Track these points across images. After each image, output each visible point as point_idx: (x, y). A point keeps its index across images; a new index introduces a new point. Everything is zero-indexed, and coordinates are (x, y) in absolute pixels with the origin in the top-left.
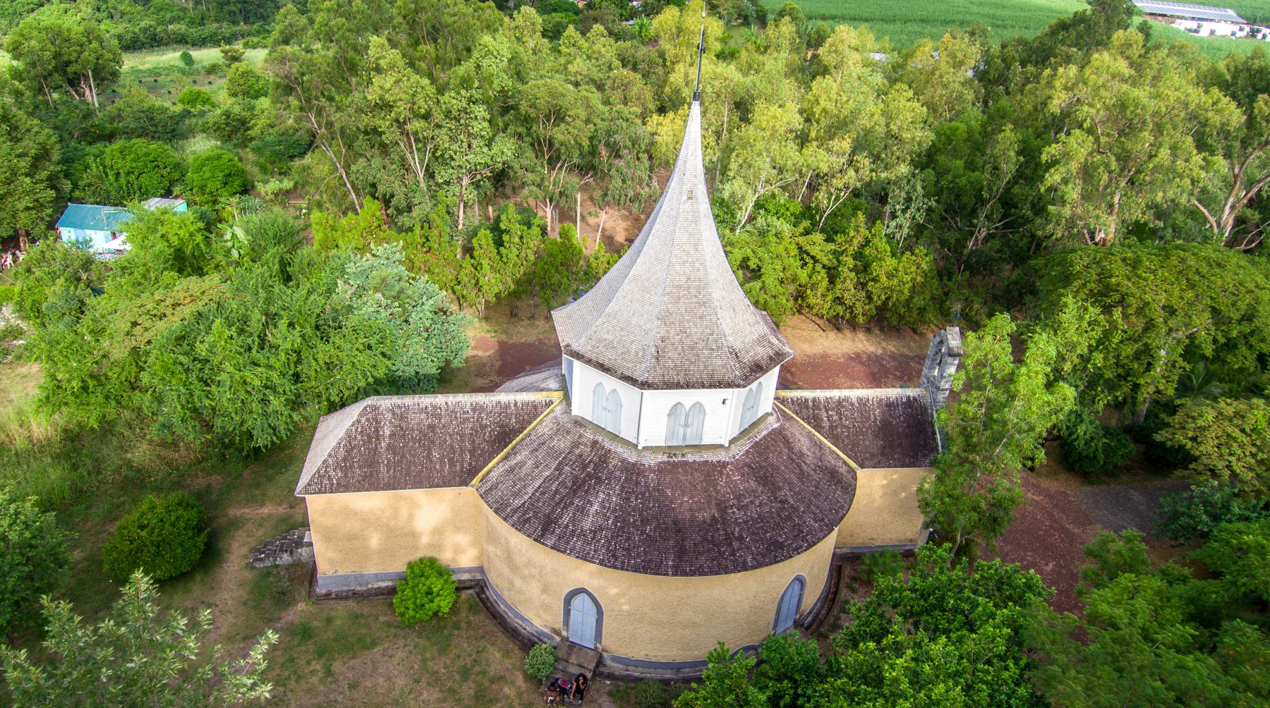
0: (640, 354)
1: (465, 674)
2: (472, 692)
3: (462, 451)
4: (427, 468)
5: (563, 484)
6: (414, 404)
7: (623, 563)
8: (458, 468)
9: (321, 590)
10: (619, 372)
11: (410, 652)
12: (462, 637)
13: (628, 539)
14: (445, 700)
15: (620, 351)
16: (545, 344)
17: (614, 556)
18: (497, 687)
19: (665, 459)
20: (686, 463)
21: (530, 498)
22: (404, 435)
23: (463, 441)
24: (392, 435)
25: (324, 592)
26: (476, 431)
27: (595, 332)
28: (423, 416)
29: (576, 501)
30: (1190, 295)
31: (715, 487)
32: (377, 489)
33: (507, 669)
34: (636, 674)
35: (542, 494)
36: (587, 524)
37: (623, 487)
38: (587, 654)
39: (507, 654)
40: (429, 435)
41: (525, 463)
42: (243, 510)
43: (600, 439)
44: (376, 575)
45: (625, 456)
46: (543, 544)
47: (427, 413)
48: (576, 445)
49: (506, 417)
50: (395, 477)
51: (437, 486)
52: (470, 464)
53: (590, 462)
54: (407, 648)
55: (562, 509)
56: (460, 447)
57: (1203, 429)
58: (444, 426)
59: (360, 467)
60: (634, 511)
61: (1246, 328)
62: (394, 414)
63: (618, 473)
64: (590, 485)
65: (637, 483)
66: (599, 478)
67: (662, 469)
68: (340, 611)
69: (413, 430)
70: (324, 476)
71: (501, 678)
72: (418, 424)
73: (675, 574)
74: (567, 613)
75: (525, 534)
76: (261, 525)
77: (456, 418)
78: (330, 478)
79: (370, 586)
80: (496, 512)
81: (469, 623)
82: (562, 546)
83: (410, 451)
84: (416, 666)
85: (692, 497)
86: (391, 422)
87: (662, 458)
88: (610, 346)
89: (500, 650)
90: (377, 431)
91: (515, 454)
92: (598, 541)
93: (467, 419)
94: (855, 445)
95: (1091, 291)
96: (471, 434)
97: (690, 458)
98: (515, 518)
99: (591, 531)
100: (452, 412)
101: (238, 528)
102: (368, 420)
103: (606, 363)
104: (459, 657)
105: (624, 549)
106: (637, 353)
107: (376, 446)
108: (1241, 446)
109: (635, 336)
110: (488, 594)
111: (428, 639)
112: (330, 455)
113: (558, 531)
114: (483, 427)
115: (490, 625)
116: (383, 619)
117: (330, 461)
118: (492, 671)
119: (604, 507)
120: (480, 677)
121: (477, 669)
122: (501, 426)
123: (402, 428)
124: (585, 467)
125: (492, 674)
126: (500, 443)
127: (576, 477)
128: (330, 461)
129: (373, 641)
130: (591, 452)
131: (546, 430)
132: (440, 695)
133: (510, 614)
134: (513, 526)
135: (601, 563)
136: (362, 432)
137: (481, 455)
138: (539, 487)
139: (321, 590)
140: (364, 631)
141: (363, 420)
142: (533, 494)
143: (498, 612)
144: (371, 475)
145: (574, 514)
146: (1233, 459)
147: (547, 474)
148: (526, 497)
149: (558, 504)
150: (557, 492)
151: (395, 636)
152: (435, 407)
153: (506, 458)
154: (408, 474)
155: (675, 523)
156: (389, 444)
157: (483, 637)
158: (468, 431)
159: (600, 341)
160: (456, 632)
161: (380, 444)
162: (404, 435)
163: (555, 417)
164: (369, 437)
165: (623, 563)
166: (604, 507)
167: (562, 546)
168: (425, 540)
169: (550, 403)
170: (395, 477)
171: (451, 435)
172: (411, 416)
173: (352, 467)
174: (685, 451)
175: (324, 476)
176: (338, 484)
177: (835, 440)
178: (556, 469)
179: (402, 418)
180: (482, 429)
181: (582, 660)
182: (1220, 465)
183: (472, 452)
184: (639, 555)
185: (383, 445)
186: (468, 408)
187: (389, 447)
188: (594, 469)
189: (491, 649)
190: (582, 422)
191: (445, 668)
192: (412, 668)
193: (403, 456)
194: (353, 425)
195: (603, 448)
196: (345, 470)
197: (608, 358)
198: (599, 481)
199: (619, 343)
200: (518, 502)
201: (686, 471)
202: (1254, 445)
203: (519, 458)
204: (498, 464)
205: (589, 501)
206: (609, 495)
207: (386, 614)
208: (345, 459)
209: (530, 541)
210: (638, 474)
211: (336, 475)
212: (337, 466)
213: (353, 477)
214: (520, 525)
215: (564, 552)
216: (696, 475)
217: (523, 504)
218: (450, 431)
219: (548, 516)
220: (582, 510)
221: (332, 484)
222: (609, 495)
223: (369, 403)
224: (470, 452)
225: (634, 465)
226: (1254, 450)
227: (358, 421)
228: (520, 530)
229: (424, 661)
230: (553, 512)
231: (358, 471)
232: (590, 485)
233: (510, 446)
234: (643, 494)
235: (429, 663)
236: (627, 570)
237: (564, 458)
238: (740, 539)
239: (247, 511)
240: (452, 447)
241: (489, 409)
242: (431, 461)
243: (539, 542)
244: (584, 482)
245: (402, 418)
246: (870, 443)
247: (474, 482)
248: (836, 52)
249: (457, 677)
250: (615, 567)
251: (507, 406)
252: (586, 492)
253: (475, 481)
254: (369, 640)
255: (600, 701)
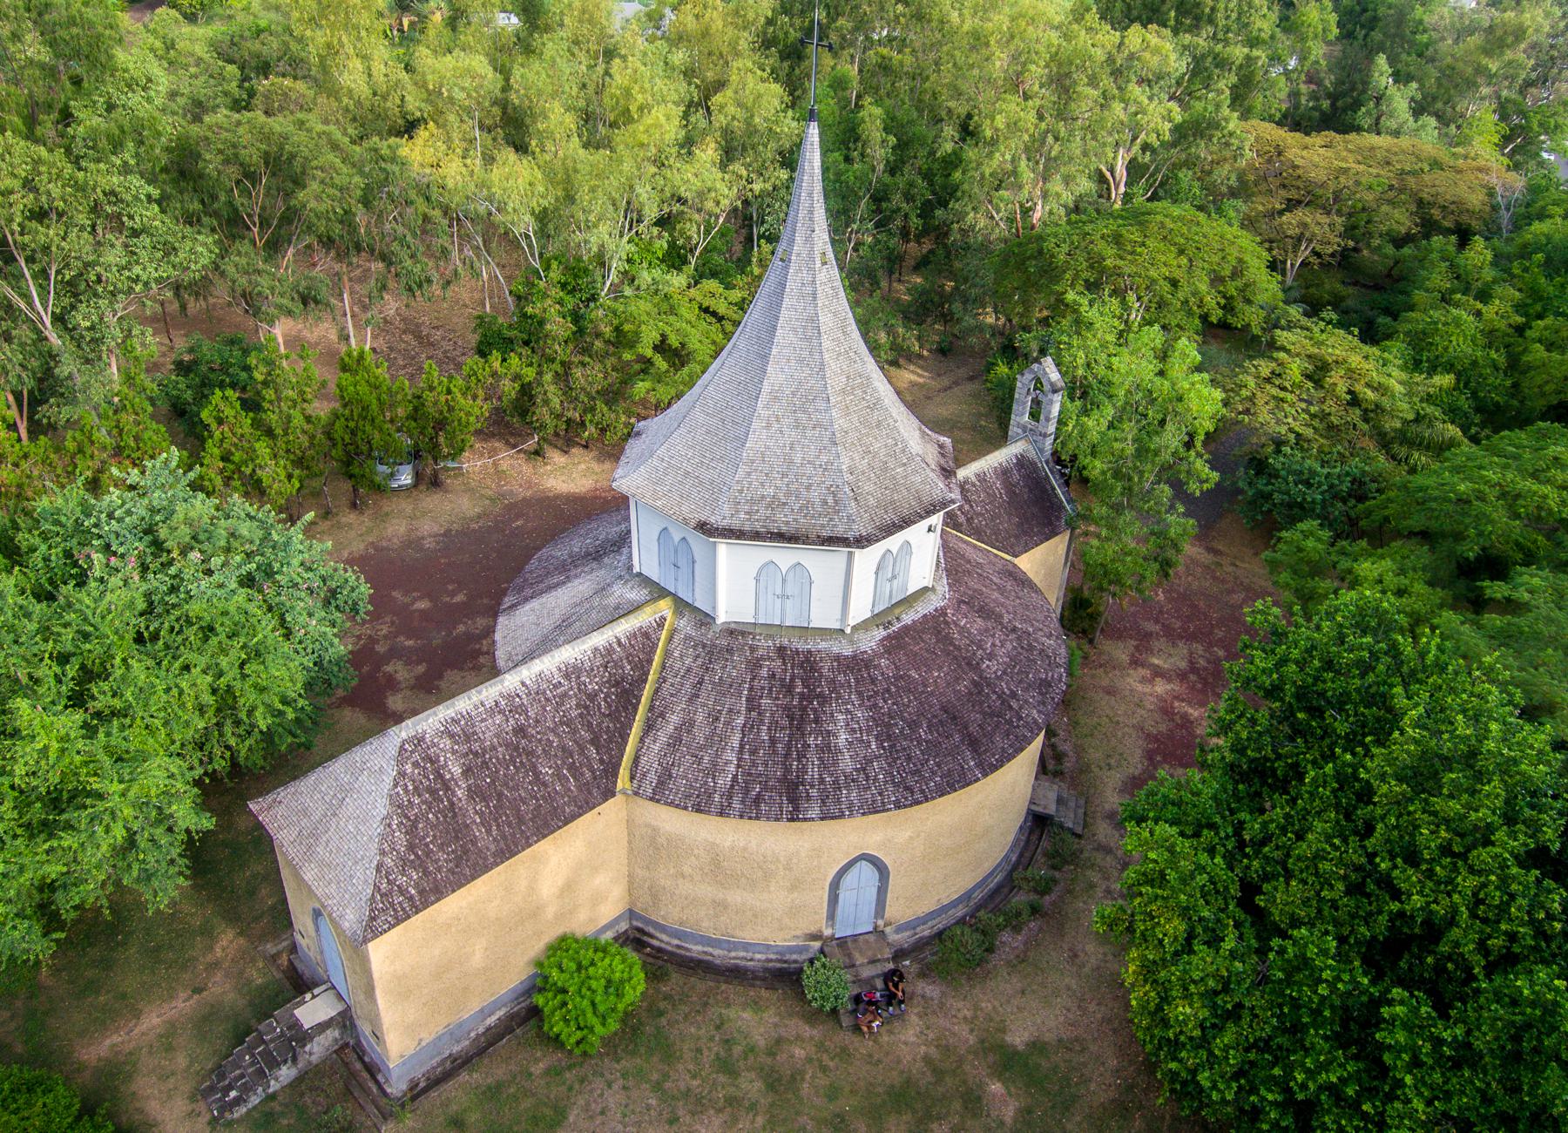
0: (830, 501)
1: (727, 1067)
2: (758, 1085)
3: (582, 749)
4: (543, 797)
5: (774, 726)
6: (476, 708)
7: (922, 791)
8: (588, 775)
9: (397, 1086)
10: (813, 536)
11: (624, 1088)
12: (677, 1022)
13: (909, 758)
14: (735, 1120)
15: (796, 508)
16: (387, 549)
17: (907, 788)
18: (785, 1056)
19: (884, 633)
20: (906, 628)
21: (738, 766)
22: (484, 762)
23: (574, 731)
24: (467, 772)
25: (404, 1087)
26: (586, 707)
27: (741, 491)
28: (498, 719)
29: (811, 741)
30: (1184, 261)
31: (952, 644)
32: (487, 869)
33: (776, 1025)
34: (926, 933)
35: (753, 752)
36: (847, 763)
37: (860, 694)
38: (867, 941)
39: (756, 1005)
40: (521, 744)
41: (692, 723)
42: (108, 1042)
43: (786, 642)
44: (482, 1010)
45: (836, 650)
46: (805, 820)
47: (501, 712)
48: (755, 665)
49: (616, 666)
50: (504, 837)
51: (574, 817)
52: (602, 761)
53: (792, 679)
54: (615, 1087)
55: (799, 760)
56: (575, 741)
57: (1251, 399)
58: (537, 721)
59: (441, 847)
60: (892, 718)
61: (1239, 283)
62: (452, 736)
63: (841, 678)
64: (815, 710)
65: (873, 681)
66: (821, 695)
67: (895, 643)
68: (457, 1093)
69: (493, 748)
70: (391, 891)
71: (779, 1041)
72: (497, 735)
73: (985, 775)
74: (833, 899)
75: (768, 819)
76: (169, 1048)
77: (547, 700)
78: (402, 891)
79: (473, 1034)
80: (699, 811)
81: (667, 997)
82: (834, 810)
83: (506, 784)
84: (653, 1102)
85: (940, 669)
86: (454, 752)
87: (880, 633)
88: (775, 504)
89: (745, 1006)
90: (440, 776)
91: (662, 715)
92: (875, 780)
93: (565, 695)
94: (996, 533)
95: (1086, 281)
96: (581, 715)
97: (908, 618)
98: (736, 805)
99: (857, 770)
100: (537, 694)
101: (129, 1077)
102: (416, 765)
103: (784, 529)
104: (699, 1050)
105: (913, 773)
106: (825, 502)
107: (452, 804)
108: (1292, 405)
109: (809, 478)
110: (655, 943)
111: (634, 1053)
112: (383, 853)
113: (814, 792)
114: (592, 697)
115: (700, 985)
116: (538, 1069)
117: (389, 862)
118: (760, 1039)
119: (853, 731)
120: (751, 1057)
121: (737, 1050)
122: (617, 684)
123: (476, 754)
124: (789, 689)
125: (762, 1043)
126: (625, 709)
127: (787, 708)
128: (389, 862)
129: (555, 1108)
130: (784, 663)
131: (688, 661)
132: (723, 1117)
133: (717, 952)
134: (741, 817)
135: (898, 806)
136: (416, 788)
137: (610, 740)
138: (742, 747)
139: (397, 1086)
140: (527, 1103)
141: (409, 768)
142: (739, 759)
143: (692, 960)
144: (466, 852)
145: (820, 759)
146: (1290, 420)
147: (740, 721)
148: (732, 768)
149: (787, 755)
150: (773, 741)
151: (582, 1081)
152: (510, 697)
153: (649, 727)
154: (521, 820)
155: (944, 709)
156: (469, 789)
157: (706, 1004)
158: (574, 713)
159: (752, 501)
160: (663, 1021)
161: (454, 793)
162: (484, 762)
163: (688, 638)
164: (433, 792)
165: (922, 791)
166: (853, 731)
167: (834, 810)
168: (550, 912)
169: (661, 623)
170: (504, 837)
171: (553, 731)
172: (480, 727)
173: (428, 853)
174: (897, 611)
175: (391, 891)
176: (421, 892)
177: (978, 534)
178: (749, 710)
179: (468, 737)
180: (592, 701)
181: (870, 953)
182: (1283, 430)
183: (595, 741)
184: (934, 773)
185: (459, 793)
186: (558, 678)
187: (473, 793)
188: (804, 686)
189: (732, 1013)
190: (740, 628)
191: (694, 1077)
192: (648, 1108)
193: (500, 795)
194: (396, 786)
195: (797, 652)
196: (420, 864)
197: (783, 520)
198: (824, 700)
199: (788, 494)
200: (724, 781)
201: (913, 638)
202: (1301, 400)
203: (674, 719)
204: (642, 740)
205: (828, 732)
206: (848, 712)
207: (537, 1060)
208: (411, 847)
209: (784, 824)
210: (867, 667)
211: (410, 880)
212: (404, 864)
213: (439, 869)
214: (753, 809)
215: (842, 816)
216: (926, 637)
217: (735, 777)
218: (550, 724)
219: (784, 780)
220: (827, 749)
221: (411, 898)
222: (848, 712)
223: (404, 735)
224: (592, 742)
225: (854, 657)
226: (1304, 405)
227: (402, 774)
228: (757, 818)
229: (658, 1087)
230: (787, 770)
231: (442, 856)
232: (815, 710)
233: (642, 709)
234: (888, 690)
235: (668, 1085)
236: (933, 798)
237: (751, 689)
238: (1014, 695)
239: (116, 1039)
240: (564, 748)
241: (587, 665)
242: (545, 784)
243: (798, 819)
244: (804, 709)
245: (468, 737)
246: (1006, 524)
247: (620, 785)
248: (590, 21)
249: (722, 1078)
250: (918, 803)
251: (609, 650)
252: (816, 721)
253: (623, 781)
254: (548, 1112)
255: (919, 990)
